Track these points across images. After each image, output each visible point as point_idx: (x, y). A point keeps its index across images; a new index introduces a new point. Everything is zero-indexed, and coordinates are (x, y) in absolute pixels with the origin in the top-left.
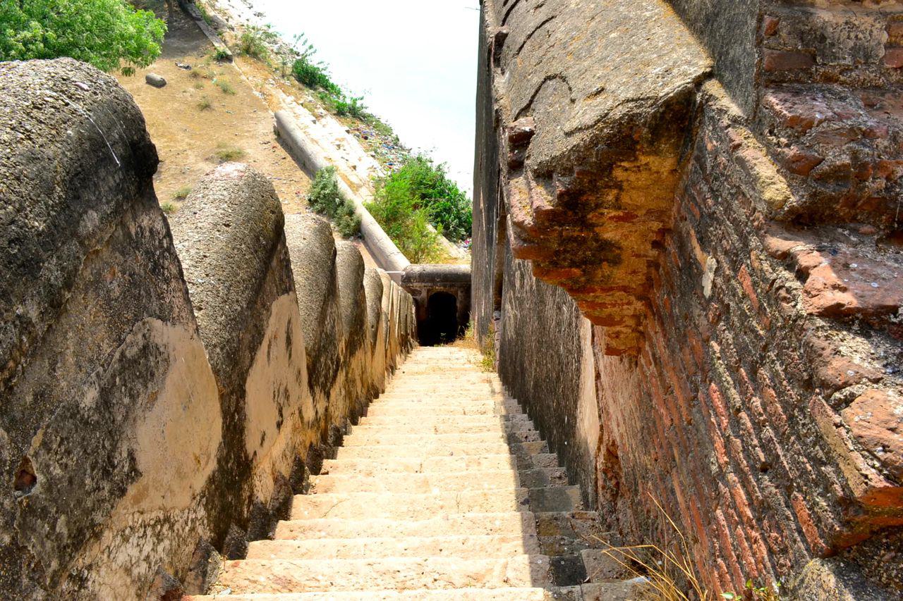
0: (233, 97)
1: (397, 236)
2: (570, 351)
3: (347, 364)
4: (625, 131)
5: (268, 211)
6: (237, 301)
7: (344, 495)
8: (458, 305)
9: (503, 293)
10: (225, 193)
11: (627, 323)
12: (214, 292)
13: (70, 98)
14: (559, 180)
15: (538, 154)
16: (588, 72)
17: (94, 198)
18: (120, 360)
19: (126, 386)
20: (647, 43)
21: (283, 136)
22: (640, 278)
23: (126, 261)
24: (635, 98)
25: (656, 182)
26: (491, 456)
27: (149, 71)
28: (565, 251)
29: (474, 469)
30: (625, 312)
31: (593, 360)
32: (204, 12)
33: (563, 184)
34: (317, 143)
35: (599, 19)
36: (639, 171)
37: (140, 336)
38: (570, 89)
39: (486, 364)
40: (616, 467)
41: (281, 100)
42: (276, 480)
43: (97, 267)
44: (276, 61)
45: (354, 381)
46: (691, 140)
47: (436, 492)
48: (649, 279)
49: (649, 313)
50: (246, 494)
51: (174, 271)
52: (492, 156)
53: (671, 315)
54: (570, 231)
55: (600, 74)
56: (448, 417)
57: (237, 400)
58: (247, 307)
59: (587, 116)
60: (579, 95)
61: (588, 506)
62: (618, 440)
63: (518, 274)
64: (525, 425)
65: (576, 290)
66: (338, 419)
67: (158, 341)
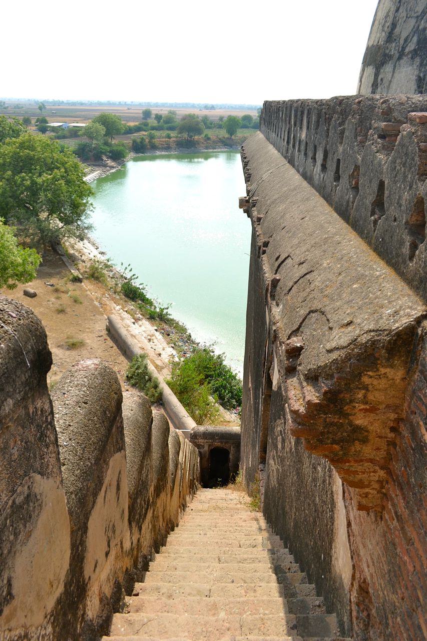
0: (81, 305)
1: (187, 404)
2: (324, 502)
3: (154, 503)
4: (369, 351)
5: (113, 393)
6: (89, 459)
7: (152, 615)
8: (231, 456)
9: (268, 451)
10: (85, 380)
11: (374, 486)
12: (74, 452)
13: (4, 322)
14: (323, 383)
15: (307, 363)
16: (340, 310)
17: (11, 390)
18: (12, 506)
19: (12, 526)
20: (380, 292)
21: (112, 333)
22: (382, 453)
23: (24, 433)
24: (375, 329)
25: (391, 386)
26: (263, 584)
27: (27, 287)
28: (328, 432)
29: (251, 596)
30: (372, 479)
31: (344, 511)
32: (67, 251)
33: (327, 385)
34: (135, 337)
35: (344, 275)
36: (380, 378)
37: (26, 488)
38: (328, 320)
39: (254, 505)
40: (367, 601)
41: (112, 308)
42: (101, 600)
43: (7, 438)
44: (111, 283)
45: (158, 517)
46: (416, 359)
47: (222, 615)
48: (388, 453)
49: (390, 480)
50: (80, 613)
51: (53, 438)
52: (259, 351)
53: (408, 483)
54: (332, 418)
55: (349, 311)
56: (228, 548)
57: (82, 534)
58: (95, 463)
59: (342, 340)
60: (335, 325)
61: (345, 633)
62: (369, 578)
63: (280, 438)
64: (288, 559)
65: (336, 461)
66: (146, 548)
67: (37, 491)
